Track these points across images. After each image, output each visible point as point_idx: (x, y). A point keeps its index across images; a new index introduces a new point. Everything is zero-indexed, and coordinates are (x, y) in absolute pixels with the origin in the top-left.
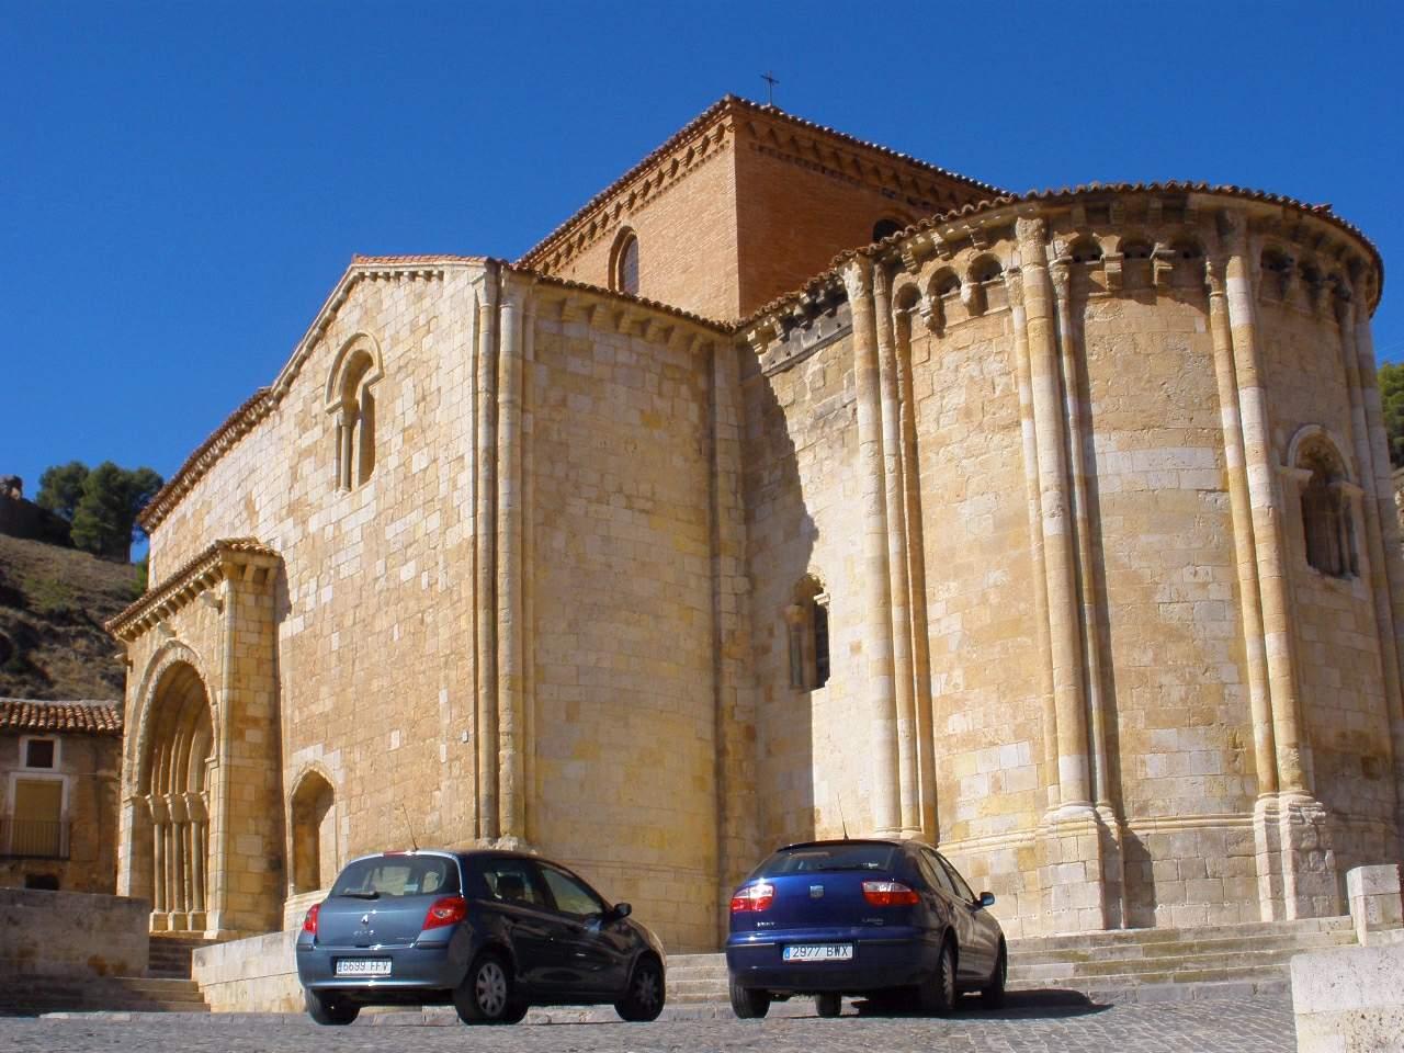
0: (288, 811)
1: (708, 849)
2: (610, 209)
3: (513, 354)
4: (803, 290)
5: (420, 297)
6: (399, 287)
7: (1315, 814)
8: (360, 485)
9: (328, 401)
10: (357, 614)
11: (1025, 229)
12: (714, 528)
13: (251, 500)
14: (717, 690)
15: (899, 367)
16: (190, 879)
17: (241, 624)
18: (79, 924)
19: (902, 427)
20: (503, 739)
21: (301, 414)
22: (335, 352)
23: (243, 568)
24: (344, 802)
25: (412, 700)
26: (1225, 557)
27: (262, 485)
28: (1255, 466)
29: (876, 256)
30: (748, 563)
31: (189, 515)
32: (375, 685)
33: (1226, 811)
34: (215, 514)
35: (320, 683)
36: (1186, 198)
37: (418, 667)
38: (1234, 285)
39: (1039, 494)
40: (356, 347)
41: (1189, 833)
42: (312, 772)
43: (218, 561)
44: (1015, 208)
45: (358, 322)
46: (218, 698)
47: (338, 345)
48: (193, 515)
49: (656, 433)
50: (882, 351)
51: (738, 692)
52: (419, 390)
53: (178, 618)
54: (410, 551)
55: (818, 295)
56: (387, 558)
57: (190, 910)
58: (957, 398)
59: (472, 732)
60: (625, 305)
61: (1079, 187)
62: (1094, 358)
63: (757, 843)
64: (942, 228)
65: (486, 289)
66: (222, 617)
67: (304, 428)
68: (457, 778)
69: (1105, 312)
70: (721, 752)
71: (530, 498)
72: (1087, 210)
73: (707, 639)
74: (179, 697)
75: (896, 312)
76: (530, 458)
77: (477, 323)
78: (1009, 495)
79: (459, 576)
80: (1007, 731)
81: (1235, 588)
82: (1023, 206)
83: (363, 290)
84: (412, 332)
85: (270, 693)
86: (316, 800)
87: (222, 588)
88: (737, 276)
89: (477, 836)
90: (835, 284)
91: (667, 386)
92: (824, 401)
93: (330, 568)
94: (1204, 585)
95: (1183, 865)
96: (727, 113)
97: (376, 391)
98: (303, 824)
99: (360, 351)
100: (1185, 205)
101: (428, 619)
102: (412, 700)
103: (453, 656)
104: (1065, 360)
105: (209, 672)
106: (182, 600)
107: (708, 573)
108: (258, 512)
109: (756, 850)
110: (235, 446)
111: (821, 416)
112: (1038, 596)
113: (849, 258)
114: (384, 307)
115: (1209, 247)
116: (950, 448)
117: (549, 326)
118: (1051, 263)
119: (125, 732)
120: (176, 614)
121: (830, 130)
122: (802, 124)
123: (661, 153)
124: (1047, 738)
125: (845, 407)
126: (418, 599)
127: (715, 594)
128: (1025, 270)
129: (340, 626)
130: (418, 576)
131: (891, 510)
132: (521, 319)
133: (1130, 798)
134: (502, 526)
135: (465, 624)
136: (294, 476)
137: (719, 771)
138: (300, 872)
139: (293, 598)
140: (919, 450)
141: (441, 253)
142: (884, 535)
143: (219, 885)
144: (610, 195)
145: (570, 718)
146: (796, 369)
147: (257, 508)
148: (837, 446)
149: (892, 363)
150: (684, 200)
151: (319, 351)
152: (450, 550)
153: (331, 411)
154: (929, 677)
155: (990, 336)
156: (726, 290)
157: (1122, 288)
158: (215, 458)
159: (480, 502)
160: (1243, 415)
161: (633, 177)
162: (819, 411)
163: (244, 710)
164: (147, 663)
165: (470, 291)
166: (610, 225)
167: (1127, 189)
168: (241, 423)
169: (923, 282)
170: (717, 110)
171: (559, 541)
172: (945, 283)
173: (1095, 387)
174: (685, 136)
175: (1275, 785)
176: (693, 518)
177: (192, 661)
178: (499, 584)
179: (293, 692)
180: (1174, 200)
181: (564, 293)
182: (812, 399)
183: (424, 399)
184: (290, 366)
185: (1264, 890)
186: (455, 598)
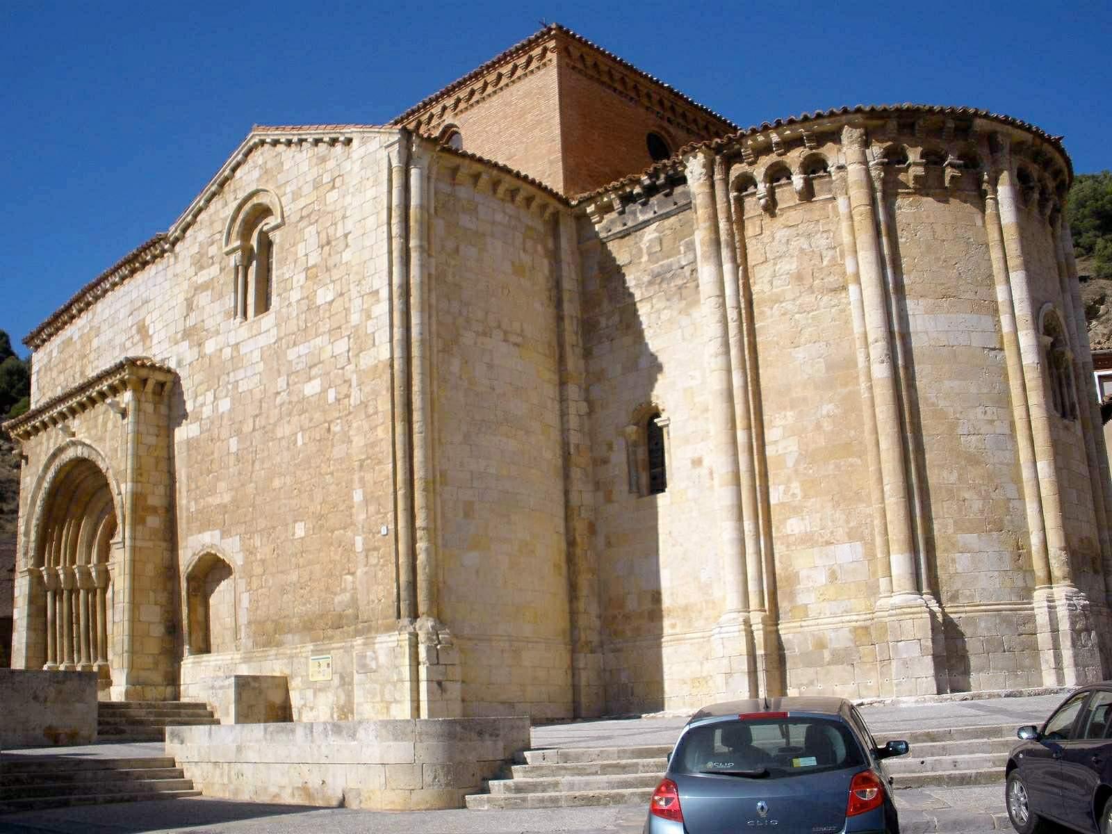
0: (184, 585)
1: (562, 623)
2: (436, 110)
3: (422, 207)
4: (646, 173)
5: (323, 160)
6: (301, 151)
7: (1083, 602)
8: (255, 316)
9: (227, 244)
10: (257, 422)
11: (848, 134)
12: (561, 359)
13: (144, 326)
14: (566, 493)
15: (737, 238)
16: (79, 637)
17: (143, 428)
18: (36, 698)
19: (741, 286)
20: (419, 534)
21: (198, 256)
22: (234, 205)
23: (145, 381)
24: (244, 580)
25: (318, 497)
26: (1004, 401)
27: (156, 314)
28: (1025, 332)
29: (718, 149)
30: (587, 390)
31: (75, 338)
32: (277, 483)
33: (1014, 599)
34: (104, 338)
35: (217, 479)
36: (972, 122)
37: (324, 468)
38: (1004, 191)
39: (867, 346)
40: (255, 200)
41: (991, 616)
42: (208, 554)
43: (125, 375)
44: (844, 118)
45: (258, 180)
46: (122, 490)
47: (236, 199)
48: (81, 337)
49: (522, 280)
50: (723, 225)
51: (583, 495)
52: (323, 236)
53: (77, 422)
54: (314, 371)
55: (658, 178)
56: (288, 376)
57: (79, 661)
58: (789, 266)
59: (392, 527)
60: (503, 175)
61: (896, 105)
62: (903, 240)
63: (599, 617)
64: (780, 129)
65: (399, 152)
66: (126, 421)
67: (199, 265)
68: (376, 565)
69: (910, 205)
70: (571, 543)
71: (434, 328)
72: (899, 125)
73: (558, 452)
74: (78, 489)
75: (733, 194)
76: (434, 296)
77: (390, 180)
78: (838, 344)
79: (375, 393)
80: (840, 532)
81: (1012, 425)
82: (851, 116)
83: (262, 154)
84: (316, 188)
85: (165, 486)
86: (206, 576)
87: (127, 397)
88: (561, 164)
89: (399, 616)
90: (675, 169)
91: (529, 244)
92: (661, 263)
93: (228, 383)
94: (991, 422)
95: (988, 641)
96: (551, 38)
97: (276, 237)
98: (196, 596)
99: (260, 204)
100: (970, 127)
101: (336, 428)
102: (318, 497)
103: (369, 461)
104: (884, 240)
105: (113, 467)
106: (83, 407)
107: (558, 398)
108: (151, 336)
109: (597, 623)
110: (126, 282)
111: (658, 275)
112: (868, 426)
113: (696, 148)
114: (286, 167)
115: (985, 161)
116: (783, 304)
117: (445, 188)
118: (871, 164)
119: (20, 514)
120: (74, 418)
121: (621, 60)
122: (603, 52)
123: (488, 67)
124: (879, 540)
125: (683, 268)
126: (324, 411)
127: (563, 414)
128: (850, 168)
129: (239, 432)
130: (324, 391)
131: (734, 352)
132: (426, 179)
133: (945, 588)
134: (415, 351)
135: (383, 433)
136: (190, 307)
137: (570, 559)
138: (193, 638)
139: (189, 407)
140: (755, 304)
141: (348, 122)
142: (729, 371)
143: (126, 648)
144: (437, 99)
145: (467, 515)
146: (632, 237)
147: (151, 332)
148: (675, 299)
149: (732, 235)
150: (508, 104)
151: (216, 204)
152: (364, 371)
153: (228, 254)
154: (767, 488)
155: (817, 218)
156: (549, 175)
157: (923, 187)
158: (105, 292)
159: (395, 330)
160: (1014, 292)
161: (461, 85)
162: (656, 271)
163: (146, 500)
164: (44, 459)
165: (384, 153)
166: (434, 123)
167: (931, 110)
168: (135, 263)
169: (759, 172)
170: (543, 34)
171: (455, 365)
172: (778, 174)
173: (905, 263)
174: (511, 54)
175: (1050, 579)
176: (547, 352)
177: (93, 457)
178: (414, 400)
179: (188, 485)
180: (962, 123)
181: (458, 161)
182: (649, 260)
183: (328, 243)
184: (188, 215)
185: (1047, 662)
186: (371, 411)
